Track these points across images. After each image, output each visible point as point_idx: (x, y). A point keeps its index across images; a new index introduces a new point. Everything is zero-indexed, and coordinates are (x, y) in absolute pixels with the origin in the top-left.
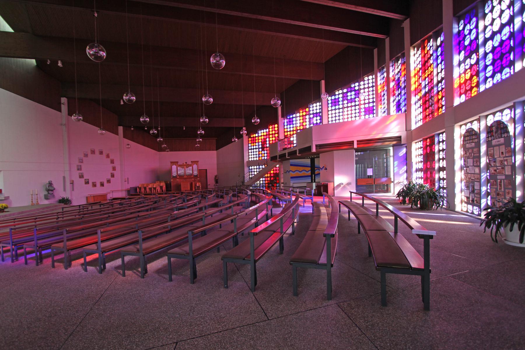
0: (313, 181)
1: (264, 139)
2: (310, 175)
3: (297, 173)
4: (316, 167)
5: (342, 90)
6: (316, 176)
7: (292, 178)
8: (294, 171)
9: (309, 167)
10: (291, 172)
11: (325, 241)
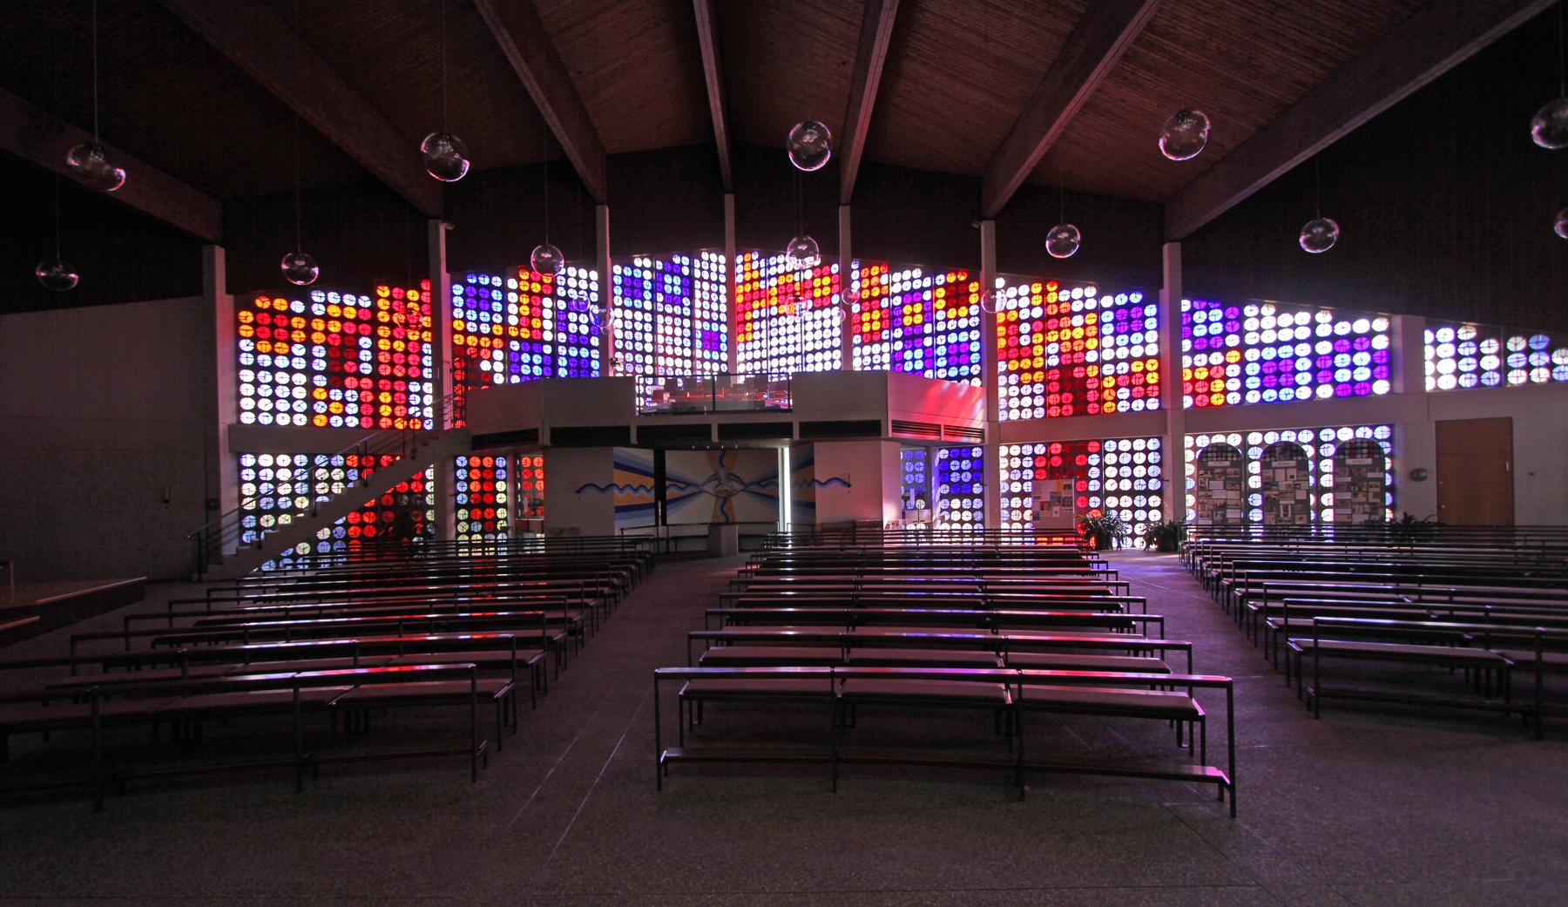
1: (342, 333)
4: (669, 479)
5: (651, 260)
6: (668, 507)
7: (620, 509)
8: (823, 481)
9: (646, 473)
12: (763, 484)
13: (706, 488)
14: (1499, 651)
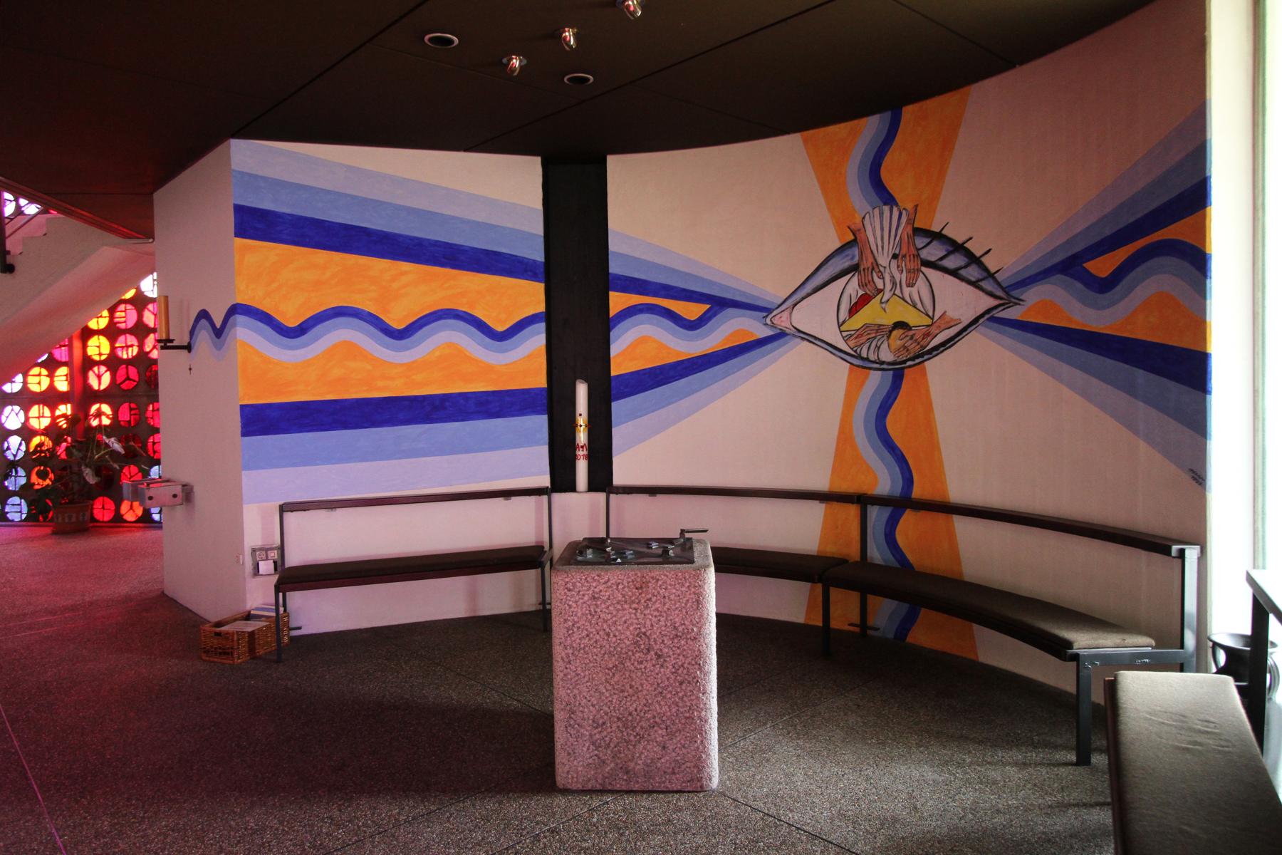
0: (582, 467)
2: (540, 381)
3: (351, 350)
6: (618, 408)
8: (291, 316)
10: (245, 333)
11: (935, 348)
12: (1101, 267)
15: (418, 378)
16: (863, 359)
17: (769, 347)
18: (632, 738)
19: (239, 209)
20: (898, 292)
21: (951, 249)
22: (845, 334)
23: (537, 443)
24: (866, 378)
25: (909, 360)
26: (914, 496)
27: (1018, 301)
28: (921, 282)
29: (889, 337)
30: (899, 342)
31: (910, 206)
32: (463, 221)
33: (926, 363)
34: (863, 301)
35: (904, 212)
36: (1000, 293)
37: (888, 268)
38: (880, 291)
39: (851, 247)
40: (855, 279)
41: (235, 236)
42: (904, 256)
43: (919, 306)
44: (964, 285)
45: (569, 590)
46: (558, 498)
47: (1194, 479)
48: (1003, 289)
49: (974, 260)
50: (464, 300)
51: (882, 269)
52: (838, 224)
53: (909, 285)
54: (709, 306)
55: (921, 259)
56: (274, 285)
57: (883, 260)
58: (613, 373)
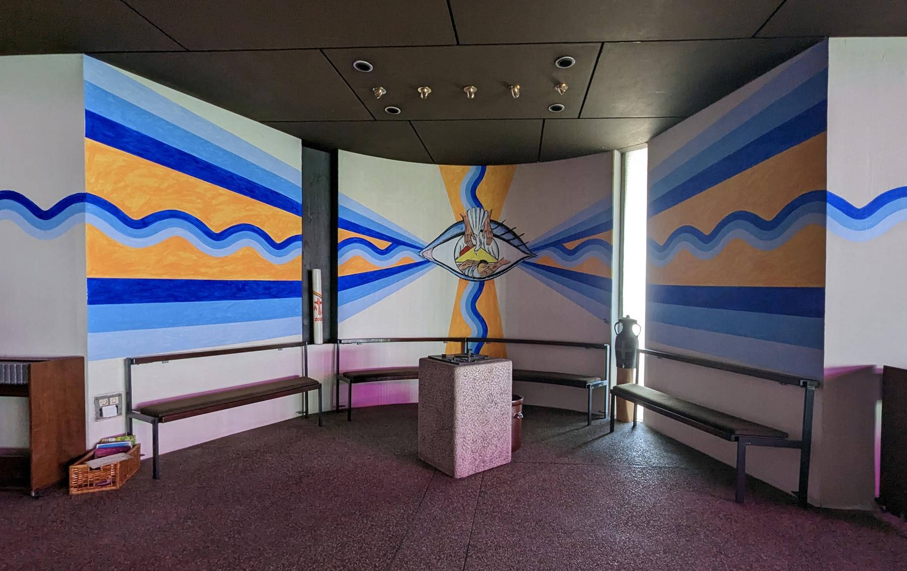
6: (341, 294)
10: (92, 218)
12: (570, 246)
13: (439, 254)
14: (639, 331)
15: (229, 268)
16: (466, 276)
17: (420, 267)
18: (486, 445)
19: (89, 115)
20: (483, 247)
21: (507, 231)
22: (457, 264)
23: (294, 314)
24: (494, 284)
25: (487, 277)
26: (488, 337)
27: (535, 256)
28: (493, 243)
29: (478, 266)
30: (483, 269)
31: (489, 210)
32: (258, 167)
33: (494, 279)
34: (467, 249)
35: (486, 212)
36: (528, 252)
37: (478, 236)
38: (475, 245)
39: (461, 224)
40: (463, 238)
41: (86, 136)
42: (486, 231)
43: (492, 254)
44: (512, 247)
45: (465, 376)
46: (309, 347)
47: (606, 322)
48: (529, 250)
49: (516, 237)
50: (258, 220)
51: (476, 236)
52: (456, 212)
53: (487, 244)
54: (391, 243)
55: (493, 234)
56: (121, 184)
57: (476, 232)
58: (339, 276)
